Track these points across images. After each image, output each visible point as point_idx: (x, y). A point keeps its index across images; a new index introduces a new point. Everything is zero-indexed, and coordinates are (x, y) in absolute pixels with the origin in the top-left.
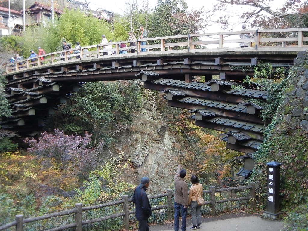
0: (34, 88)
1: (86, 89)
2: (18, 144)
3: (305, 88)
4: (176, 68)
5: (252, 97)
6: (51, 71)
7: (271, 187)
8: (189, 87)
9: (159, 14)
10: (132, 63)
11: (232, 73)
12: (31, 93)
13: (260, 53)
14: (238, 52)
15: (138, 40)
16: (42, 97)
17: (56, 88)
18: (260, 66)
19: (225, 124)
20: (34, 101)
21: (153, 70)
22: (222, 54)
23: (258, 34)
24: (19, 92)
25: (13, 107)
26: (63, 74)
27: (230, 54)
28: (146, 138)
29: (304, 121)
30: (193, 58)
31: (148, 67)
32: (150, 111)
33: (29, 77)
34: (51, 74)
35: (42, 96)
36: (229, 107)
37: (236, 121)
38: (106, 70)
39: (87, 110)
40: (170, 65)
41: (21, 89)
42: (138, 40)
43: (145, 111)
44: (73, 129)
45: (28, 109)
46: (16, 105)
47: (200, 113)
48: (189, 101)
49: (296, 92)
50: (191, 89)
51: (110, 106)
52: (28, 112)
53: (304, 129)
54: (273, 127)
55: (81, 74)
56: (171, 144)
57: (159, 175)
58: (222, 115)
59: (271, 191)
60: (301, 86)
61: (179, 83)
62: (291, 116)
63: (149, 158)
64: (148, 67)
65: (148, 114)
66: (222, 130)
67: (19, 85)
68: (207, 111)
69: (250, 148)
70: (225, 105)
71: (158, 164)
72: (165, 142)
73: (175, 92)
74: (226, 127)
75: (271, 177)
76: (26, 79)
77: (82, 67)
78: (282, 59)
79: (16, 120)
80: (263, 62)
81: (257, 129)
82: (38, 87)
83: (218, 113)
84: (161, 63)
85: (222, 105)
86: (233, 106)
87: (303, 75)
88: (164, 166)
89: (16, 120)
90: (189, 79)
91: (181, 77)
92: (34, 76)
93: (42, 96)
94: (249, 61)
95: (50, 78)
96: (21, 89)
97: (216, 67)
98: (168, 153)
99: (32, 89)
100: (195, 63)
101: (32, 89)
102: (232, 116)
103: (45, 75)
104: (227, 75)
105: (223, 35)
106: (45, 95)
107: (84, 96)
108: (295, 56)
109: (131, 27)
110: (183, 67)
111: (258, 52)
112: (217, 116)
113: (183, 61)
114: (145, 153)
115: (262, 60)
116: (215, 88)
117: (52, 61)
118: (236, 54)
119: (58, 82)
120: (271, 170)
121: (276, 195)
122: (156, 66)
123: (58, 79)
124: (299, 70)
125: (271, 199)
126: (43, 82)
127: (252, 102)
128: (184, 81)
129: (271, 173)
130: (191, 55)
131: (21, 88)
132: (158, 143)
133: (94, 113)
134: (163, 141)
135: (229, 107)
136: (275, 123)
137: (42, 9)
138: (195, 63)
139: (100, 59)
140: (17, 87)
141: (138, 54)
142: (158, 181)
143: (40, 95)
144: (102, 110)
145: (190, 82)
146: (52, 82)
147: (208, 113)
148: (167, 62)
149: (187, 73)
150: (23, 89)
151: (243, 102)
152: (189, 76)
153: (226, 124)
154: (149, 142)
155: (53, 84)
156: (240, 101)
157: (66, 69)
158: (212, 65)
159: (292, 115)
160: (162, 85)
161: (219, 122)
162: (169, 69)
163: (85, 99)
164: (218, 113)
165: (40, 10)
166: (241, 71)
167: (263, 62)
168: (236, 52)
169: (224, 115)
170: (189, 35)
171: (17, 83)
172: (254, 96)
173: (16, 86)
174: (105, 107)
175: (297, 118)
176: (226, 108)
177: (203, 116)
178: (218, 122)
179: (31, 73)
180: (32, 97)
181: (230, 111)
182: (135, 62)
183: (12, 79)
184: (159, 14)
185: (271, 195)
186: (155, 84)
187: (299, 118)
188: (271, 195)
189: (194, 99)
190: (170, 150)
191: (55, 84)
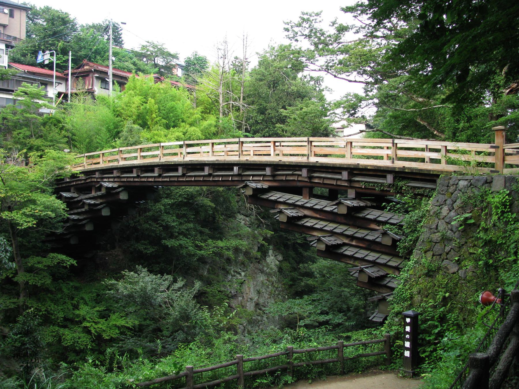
0: (93, 194)
1: (161, 193)
3: (447, 221)
5: (388, 223)
6: (118, 173)
7: (408, 340)
8: (308, 205)
9: (261, 80)
10: (232, 170)
11: (364, 191)
12: (88, 201)
14: (371, 166)
16: (104, 207)
17: (123, 196)
20: (93, 210)
21: (260, 180)
22: (351, 167)
24: (72, 198)
26: (134, 177)
27: (361, 167)
28: (241, 258)
30: (313, 168)
31: (253, 176)
32: (247, 216)
33: (87, 179)
34: (118, 177)
35: (104, 205)
36: (361, 233)
37: (369, 252)
38: (195, 176)
39: (163, 220)
40: (283, 175)
41: (75, 195)
43: (240, 217)
44: (145, 249)
45: (84, 222)
48: (308, 224)
50: (311, 209)
51: (193, 215)
52: (85, 227)
55: (160, 180)
56: (277, 263)
57: (260, 309)
59: (407, 344)
61: (294, 198)
63: (245, 287)
64: (253, 176)
65: (243, 222)
66: (351, 262)
68: (332, 238)
69: (386, 286)
70: (355, 231)
71: (259, 292)
72: (268, 261)
73: (291, 213)
74: (357, 259)
75: (408, 329)
76: (83, 182)
77: (161, 170)
78: (423, 178)
79: (68, 237)
81: (394, 263)
82: (99, 193)
83: (346, 241)
84: (272, 172)
85: (350, 231)
86: (366, 232)
88: (267, 296)
89: (68, 237)
90: (308, 194)
91: (297, 191)
92: (95, 178)
93: (104, 205)
94: (385, 177)
95: (116, 181)
96: (75, 195)
97: (343, 182)
98: (272, 277)
100: (316, 175)
102: (364, 246)
103: (109, 178)
104: (357, 193)
105: (351, 143)
106: (108, 204)
107: (158, 202)
108: (438, 176)
109: (221, 101)
110: (300, 179)
111: (395, 168)
112: (344, 244)
114: (241, 278)
115: (400, 177)
116: (343, 211)
120: (408, 320)
121: (412, 350)
122: (264, 176)
123: (127, 184)
124: (441, 198)
125: (407, 354)
126: (107, 188)
128: (302, 195)
129: (408, 324)
131: (74, 193)
132: (259, 262)
133: (173, 224)
134: (265, 260)
135: (361, 233)
138: (316, 175)
139: (186, 161)
140: (69, 191)
142: (259, 318)
143: (101, 204)
144: (182, 221)
145: (309, 199)
146: (119, 187)
147: (332, 241)
148: (279, 170)
149: (306, 187)
150: (77, 194)
152: (308, 190)
153: (356, 255)
154: (246, 261)
155: (120, 189)
156: (373, 226)
157: (140, 171)
158: (338, 180)
160: (272, 201)
162: (282, 180)
163: (159, 206)
164: (346, 241)
165: (90, 71)
166: (375, 189)
168: (368, 166)
170: (308, 139)
171: (69, 186)
172: (391, 221)
173: (68, 190)
174: (186, 218)
175: (438, 257)
177: (327, 245)
178: (347, 253)
180: (91, 207)
181: (362, 240)
182: (236, 169)
184: (261, 80)
185: (407, 349)
187: (441, 257)
188: (407, 349)
189: (315, 221)
190: (275, 272)
191: (122, 190)
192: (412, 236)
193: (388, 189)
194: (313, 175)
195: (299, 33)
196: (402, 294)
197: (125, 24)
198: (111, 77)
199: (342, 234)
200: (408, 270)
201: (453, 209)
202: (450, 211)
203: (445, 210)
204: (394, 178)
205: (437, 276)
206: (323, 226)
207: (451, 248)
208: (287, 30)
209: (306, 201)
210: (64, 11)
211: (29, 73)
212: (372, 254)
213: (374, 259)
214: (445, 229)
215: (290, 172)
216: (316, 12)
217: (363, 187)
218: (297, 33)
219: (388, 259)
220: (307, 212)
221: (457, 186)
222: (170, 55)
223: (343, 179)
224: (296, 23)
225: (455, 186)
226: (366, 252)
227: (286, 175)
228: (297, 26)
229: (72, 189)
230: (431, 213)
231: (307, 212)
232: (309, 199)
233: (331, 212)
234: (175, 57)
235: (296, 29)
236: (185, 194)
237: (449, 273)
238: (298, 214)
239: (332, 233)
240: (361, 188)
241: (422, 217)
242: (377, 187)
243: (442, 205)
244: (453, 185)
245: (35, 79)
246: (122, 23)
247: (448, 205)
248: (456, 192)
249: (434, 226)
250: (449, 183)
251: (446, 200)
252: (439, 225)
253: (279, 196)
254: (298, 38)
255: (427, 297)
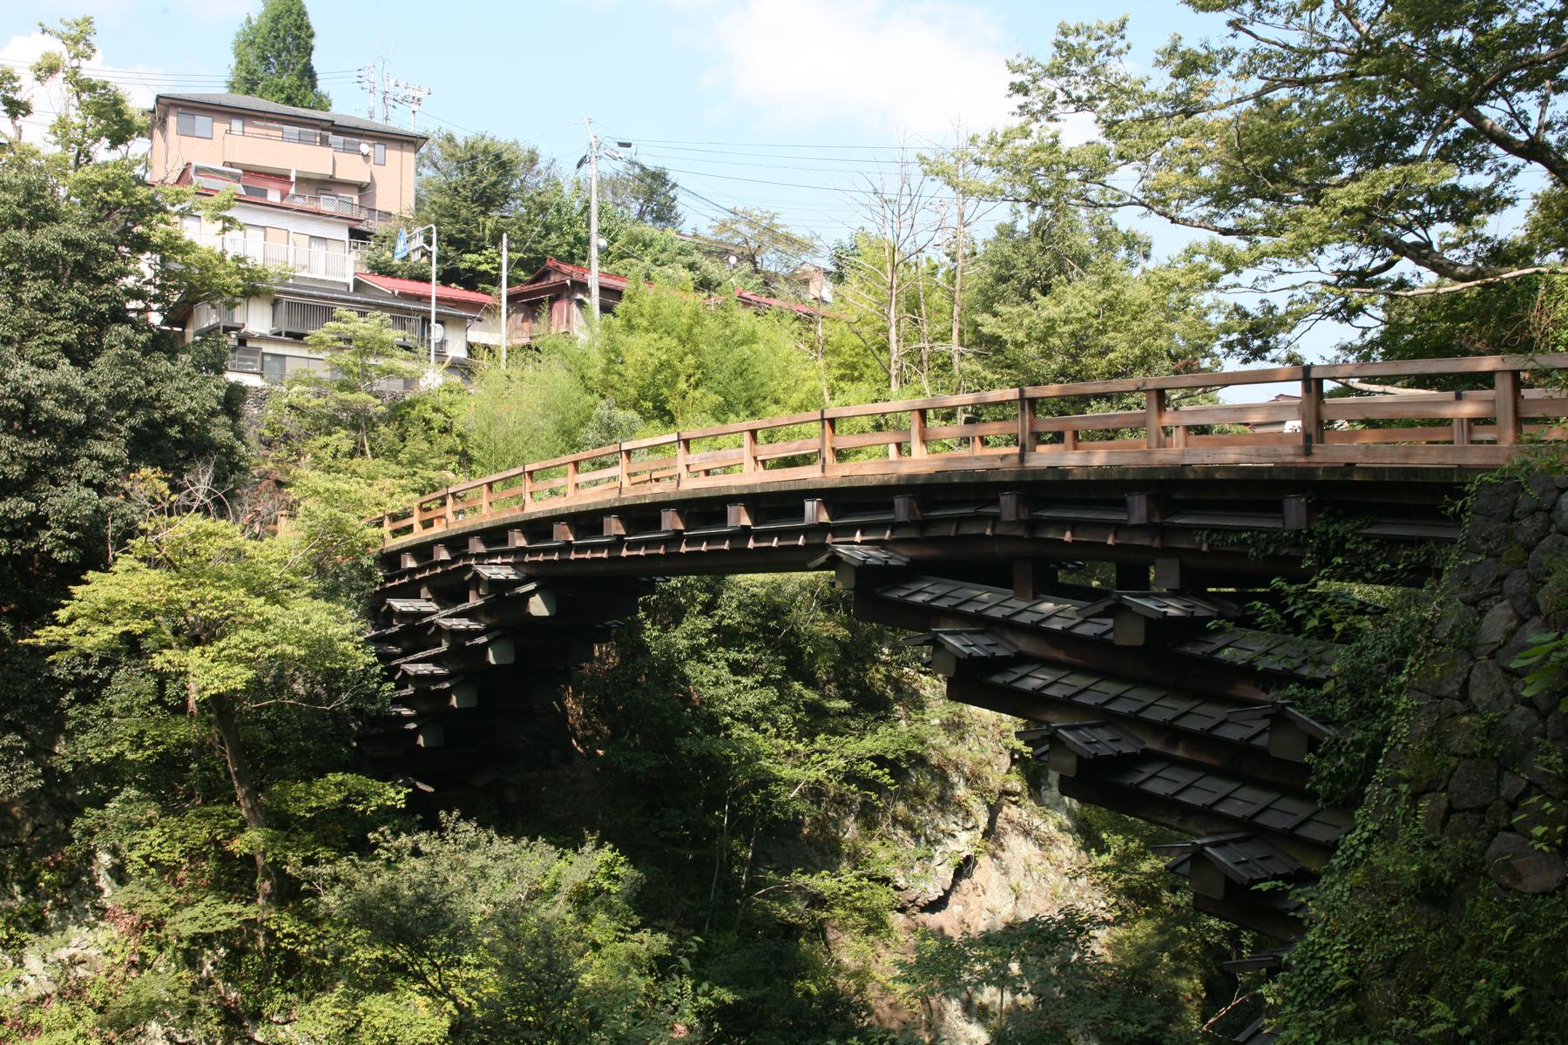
2: (443, 814)
4: (974, 532)
13: (1320, 476)
15: (822, 412)
18: (1326, 533)
19: (1183, 798)
20: (462, 652)
22: (1155, 476)
23: (1313, 384)
25: (397, 677)
29: (1510, 835)
36: (1202, 718)
37: (1234, 786)
42: (822, 412)
46: (406, 667)
47: (1068, 744)
49: (1467, 681)
53: (1507, 881)
54: (1358, 855)
58: (1170, 752)
60: (1492, 655)
61: (985, 599)
62: (1444, 805)
67: (424, 592)
68: (1104, 735)
70: (1183, 707)
74: (1189, 811)
80: (1341, 512)
84: (910, 510)
85: (1164, 710)
86: (1219, 713)
87: (1501, 595)
91: (996, 574)
94: (1276, 508)
99: (460, 607)
101: (460, 607)
104: (1184, 570)
110: (1000, 530)
112: (1147, 757)
113: (996, 502)
116: (1132, 636)
117: (528, 498)
118: (1218, 476)
119: (549, 580)
122: (894, 526)
127: (1292, 705)
128: (1011, 587)
130: (1029, 479)
131: (428, 600)
135: (1202, 718)
136: (1365, 835)
137: (568, 282)
139: (686, 491)
141: (823, 471)
147: (1103, 742)
151: (1262, 696)
156: (1246, 690)
159: (1449, 802)
161: (1158, 787)
162: (946, 539)
164: (1154, 745)
166: (1245, 555)
167: (1341, 512)
169: (1180, 753)
170: (1022, 392)
173: (411, 592)
175: (1472, 819)
176: (1187, 723)
179: (456, 543)
183: (398, 564)
184: (1003, 279)
186: (892, 601)
187: (1482, 821)
192: (1366, 729)
193: (1294, 552)
194: (1039, 513)
195: (1061, 97)
196: (1319, 970)
197: (628, 145)
198: (595, 291)
199: (1135, 721)
200: (1345, 869)
201: (1536, 611)
202: (1523, 621)
203: (1497, 619)
204: (1312, 510)
205: (1469, 903)
206: (1073, 690)
207: (1530, 783)
208: (1021, 89)
209: (1022, 605)
210: (233, 38)
211: (404, 296)
212: (1247, 793)
213: (1251, 811)
214: (1499, 697)
215: (969, 511)
216: (1106, 24)
217: (1205, 548)
218: (1053, 96)
219: (1302, 815)
220: (1025, 645)
221: (1554, 515)
222: (790, 240)
223: (1134, 521)
224: (1046, 61)
225: (1540, 517)
226: (1222, 787)
227: (960, 520)
228: (1052, 76)
229: (424, 592)
230: (1442, 633)
231: (1025, 645)
232: (1035, 597)
233: (1098, 642)
234: (804, 247)
235: (1049, 84)
236: (753, 604)
237: (1520, 894)
238: (993, 650)
239: (1104, 717)
240: (1198, 551)
241: (1405, 652)
242: (1254, 544)
243: (1488, 596)
244: (1532, 512)
245: (409, 309)
246: (622, 145)
247: (1513, 597)
248: (1546, 542)
249: (1453, 687)
250: (1515, 504)
251: (1501, 579)
252: (1473, 681)
253: (938, 591)
254: (1058, 110)
255: (1425, 990)
